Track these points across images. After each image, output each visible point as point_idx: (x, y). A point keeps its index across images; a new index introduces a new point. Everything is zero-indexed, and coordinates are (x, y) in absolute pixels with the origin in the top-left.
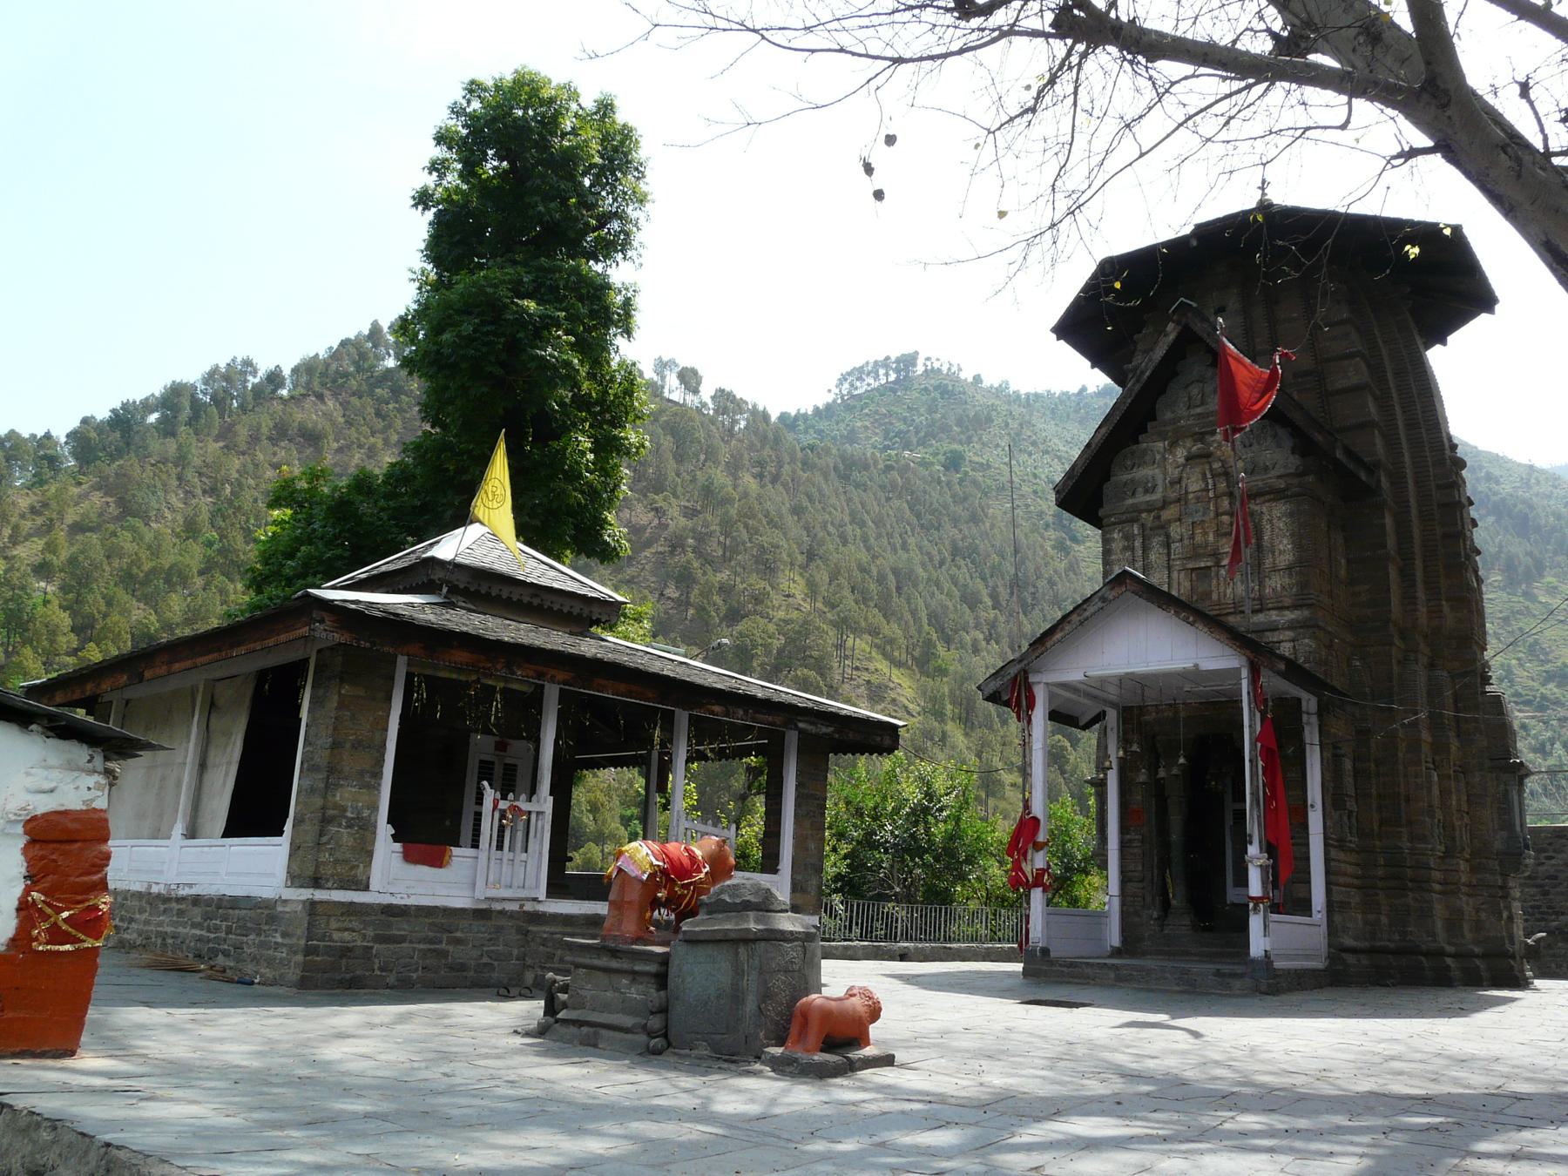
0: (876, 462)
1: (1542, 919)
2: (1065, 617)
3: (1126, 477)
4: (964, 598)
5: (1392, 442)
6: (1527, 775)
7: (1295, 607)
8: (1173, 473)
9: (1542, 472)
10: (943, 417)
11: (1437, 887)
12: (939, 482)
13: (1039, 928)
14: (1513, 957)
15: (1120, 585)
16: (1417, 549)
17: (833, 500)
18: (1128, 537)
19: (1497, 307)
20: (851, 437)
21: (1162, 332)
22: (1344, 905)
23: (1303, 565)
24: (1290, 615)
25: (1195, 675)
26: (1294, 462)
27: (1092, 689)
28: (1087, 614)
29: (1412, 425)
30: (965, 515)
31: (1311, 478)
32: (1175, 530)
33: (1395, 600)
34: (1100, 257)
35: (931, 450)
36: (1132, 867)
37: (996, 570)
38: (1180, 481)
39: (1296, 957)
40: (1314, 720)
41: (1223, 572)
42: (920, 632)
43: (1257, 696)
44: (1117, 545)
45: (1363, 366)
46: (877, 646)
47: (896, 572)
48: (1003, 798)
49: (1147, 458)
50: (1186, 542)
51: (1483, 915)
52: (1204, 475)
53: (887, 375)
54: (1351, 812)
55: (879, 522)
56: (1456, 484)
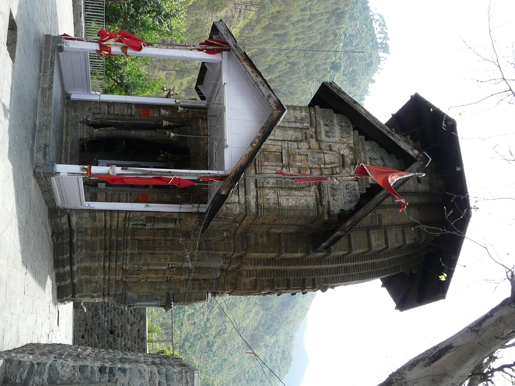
0: (339, 29)
1: (102, 307)
2: (259, 74)
3: (335, 121)
4: (270, 66)
5: (339, 259)
6: (165, 309)
7: (257, 205)
8: (336, 147)
9: (306, 313)
10: (357, 64)
11: (107, 265)
12: (326, 59)
13: (75, 46)
14: (73, 296)
15: (277, 107)
16: (283, 268)
17: (323, 6)
18: (302, 120)
19: (398, 311)
20: (352, 18)
21: (415, 148)
22: (94, 219)
23: (279, 207)
24: (253, 202)
25: (222, 145)
26: (336, 209)
27: (217, 88)
28: (261, 87)
29: (347, 269)
30: (310, 70)
31: (326, 218)
32: (304, 145)
33: (256, 255)
34: (455, 119)
35: (342, 56)
36: (116, 108)
37: (282, 82)
38: (331, 150)
39: (61, 191)
40: (195, 210)
41: (279, 169)
42: (256, 44)
43: (207, 180)
44: (299, 114)
45: (380, 249)
46: (250, 23)
47: (285, 35)
48: (176, 78)
49: (345, 134)
50: (297, 151)
51: (94, 285)
52: (333, 163)
53: (380, 38)
54: (145, 225)
55: (310, 28)
56: (314, 288)
